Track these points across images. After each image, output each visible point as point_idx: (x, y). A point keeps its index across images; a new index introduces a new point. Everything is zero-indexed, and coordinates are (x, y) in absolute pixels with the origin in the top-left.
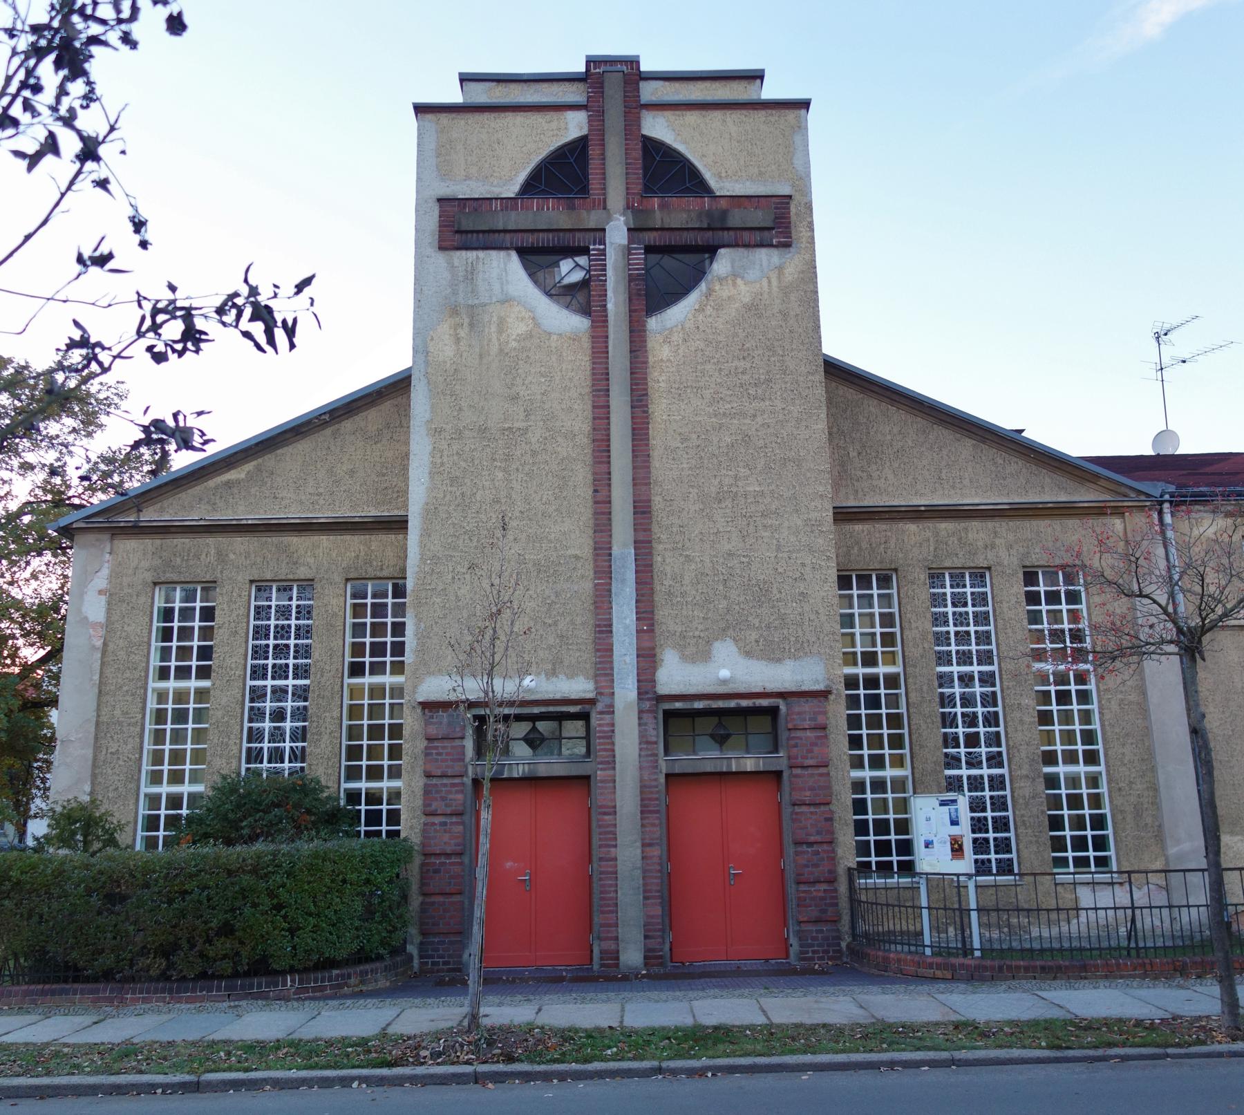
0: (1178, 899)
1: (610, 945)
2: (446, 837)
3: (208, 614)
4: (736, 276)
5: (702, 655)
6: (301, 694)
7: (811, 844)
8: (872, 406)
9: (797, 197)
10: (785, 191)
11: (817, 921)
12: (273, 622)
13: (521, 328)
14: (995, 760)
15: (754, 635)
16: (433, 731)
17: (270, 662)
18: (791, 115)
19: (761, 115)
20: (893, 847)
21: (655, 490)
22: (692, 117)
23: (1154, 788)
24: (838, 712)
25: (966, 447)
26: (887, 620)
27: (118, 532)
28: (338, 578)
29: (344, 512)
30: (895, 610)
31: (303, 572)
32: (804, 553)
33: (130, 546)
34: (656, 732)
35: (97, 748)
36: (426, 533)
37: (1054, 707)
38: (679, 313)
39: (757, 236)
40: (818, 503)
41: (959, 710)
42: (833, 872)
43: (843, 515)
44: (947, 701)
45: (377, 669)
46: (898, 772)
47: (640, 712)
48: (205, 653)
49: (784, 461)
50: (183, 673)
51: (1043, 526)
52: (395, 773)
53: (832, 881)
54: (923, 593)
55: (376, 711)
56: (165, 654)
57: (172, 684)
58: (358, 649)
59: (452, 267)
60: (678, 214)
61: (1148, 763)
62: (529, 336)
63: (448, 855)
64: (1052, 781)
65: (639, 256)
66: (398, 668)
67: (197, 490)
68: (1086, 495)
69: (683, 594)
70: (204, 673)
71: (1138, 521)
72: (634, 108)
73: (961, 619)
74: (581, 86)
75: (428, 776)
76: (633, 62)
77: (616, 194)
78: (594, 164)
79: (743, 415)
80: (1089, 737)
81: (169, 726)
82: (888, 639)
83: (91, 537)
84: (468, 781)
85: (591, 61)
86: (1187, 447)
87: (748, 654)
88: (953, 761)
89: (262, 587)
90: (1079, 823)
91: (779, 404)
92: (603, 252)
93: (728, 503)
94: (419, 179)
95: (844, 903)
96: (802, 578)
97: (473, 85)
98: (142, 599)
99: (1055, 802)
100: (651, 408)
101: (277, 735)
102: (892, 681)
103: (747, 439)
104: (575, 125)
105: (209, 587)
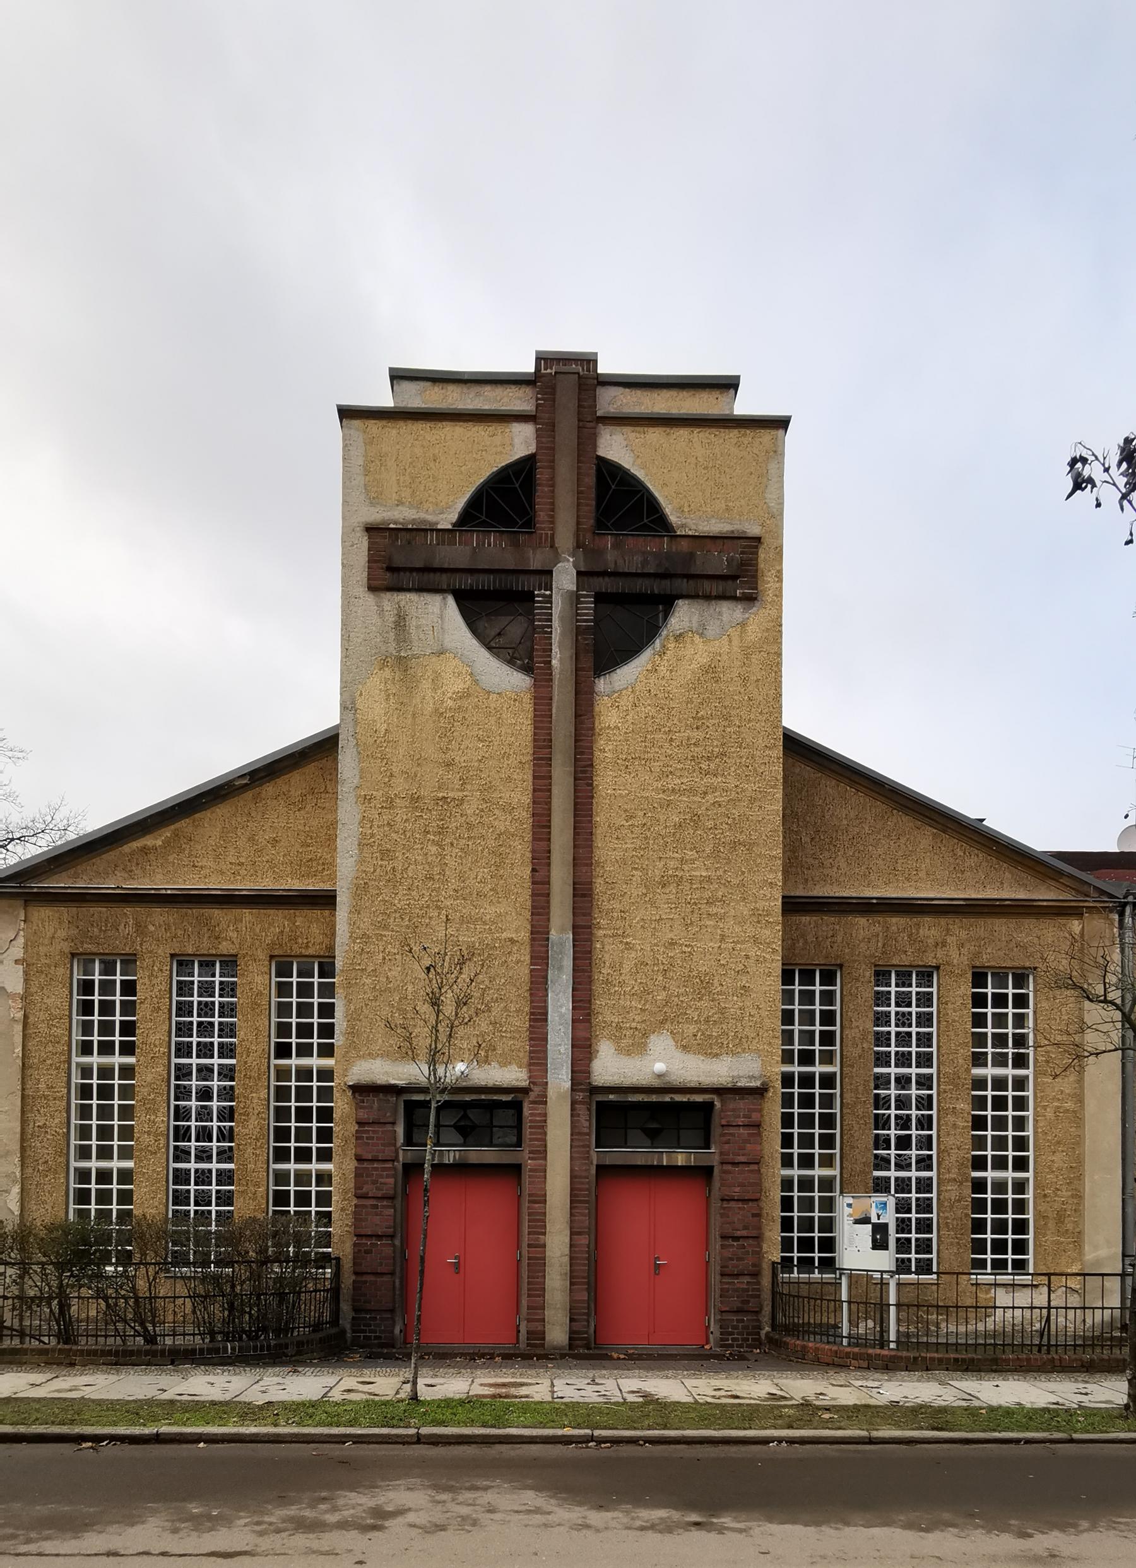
3: (129, 988)
4: (696, 633)
5: (638, 1047)
8: (830, 787)
9: (767, 540)
10: (754, 530)
11: (738, 1311)
13: (459, 686)
14: (924, 1163)
15: (692, 1029)
16: (363, 1115)
17: (195, 1040)
18: (766, 436)
19: (734, 433)
21: (599, 871)
22: (655, 435)
23: (1079, 1196)
24: (773, 1110)
25: (926, 836)
28: (262, 955)
29: (267, 883)
30: (837, 1008)
31: (225, 948)
32: (748, 948)
33: (43, 914)
34: (588, 1122)
35: (24, 1122)
36: (356, 910)
38: (628, 674)
40: (766, 891)
42: (757, 1265)
43: (792, 906)
44: (881, 1102)
45: (305, 1051)
46: (827, 1172)
47: (573, 1103)
49: (735, 845)
50: (106, 1048)
51: (1001, 926)
52: (325, 1155)
53: (756, 1274)
54: (867, 990)
55: (304, 1094)
56: (87, 1028)
57: (95, 1060)
58: (284, 1030)
59: (381, 612)
60: (630, 553)
62: (466, 695)
63: (379, 1237)
64: (979, 1186)
65: (588, 606)
66: (327, 1051)
67: (112, 855)
68: (1045, 894)
69: (621, 984)
70: (128, 1049)
72: (592, 422)
74: (527, 392)
75: (359, 1159)
76: (589, 361)
77: (565, 537)
78: (541, 491)
79: (692, 791)
84: (399, 1166)
85: (543, 359)
89: (184, 963)
91: (732, 782)
93: (672, 888)
94: (345, 502)
95: (767, 1295)
98: (61, 971)
100: (597, 780)
101: (204, 1114)
102: (828, 1081)
104: (520, 441)
105: (129, 962)
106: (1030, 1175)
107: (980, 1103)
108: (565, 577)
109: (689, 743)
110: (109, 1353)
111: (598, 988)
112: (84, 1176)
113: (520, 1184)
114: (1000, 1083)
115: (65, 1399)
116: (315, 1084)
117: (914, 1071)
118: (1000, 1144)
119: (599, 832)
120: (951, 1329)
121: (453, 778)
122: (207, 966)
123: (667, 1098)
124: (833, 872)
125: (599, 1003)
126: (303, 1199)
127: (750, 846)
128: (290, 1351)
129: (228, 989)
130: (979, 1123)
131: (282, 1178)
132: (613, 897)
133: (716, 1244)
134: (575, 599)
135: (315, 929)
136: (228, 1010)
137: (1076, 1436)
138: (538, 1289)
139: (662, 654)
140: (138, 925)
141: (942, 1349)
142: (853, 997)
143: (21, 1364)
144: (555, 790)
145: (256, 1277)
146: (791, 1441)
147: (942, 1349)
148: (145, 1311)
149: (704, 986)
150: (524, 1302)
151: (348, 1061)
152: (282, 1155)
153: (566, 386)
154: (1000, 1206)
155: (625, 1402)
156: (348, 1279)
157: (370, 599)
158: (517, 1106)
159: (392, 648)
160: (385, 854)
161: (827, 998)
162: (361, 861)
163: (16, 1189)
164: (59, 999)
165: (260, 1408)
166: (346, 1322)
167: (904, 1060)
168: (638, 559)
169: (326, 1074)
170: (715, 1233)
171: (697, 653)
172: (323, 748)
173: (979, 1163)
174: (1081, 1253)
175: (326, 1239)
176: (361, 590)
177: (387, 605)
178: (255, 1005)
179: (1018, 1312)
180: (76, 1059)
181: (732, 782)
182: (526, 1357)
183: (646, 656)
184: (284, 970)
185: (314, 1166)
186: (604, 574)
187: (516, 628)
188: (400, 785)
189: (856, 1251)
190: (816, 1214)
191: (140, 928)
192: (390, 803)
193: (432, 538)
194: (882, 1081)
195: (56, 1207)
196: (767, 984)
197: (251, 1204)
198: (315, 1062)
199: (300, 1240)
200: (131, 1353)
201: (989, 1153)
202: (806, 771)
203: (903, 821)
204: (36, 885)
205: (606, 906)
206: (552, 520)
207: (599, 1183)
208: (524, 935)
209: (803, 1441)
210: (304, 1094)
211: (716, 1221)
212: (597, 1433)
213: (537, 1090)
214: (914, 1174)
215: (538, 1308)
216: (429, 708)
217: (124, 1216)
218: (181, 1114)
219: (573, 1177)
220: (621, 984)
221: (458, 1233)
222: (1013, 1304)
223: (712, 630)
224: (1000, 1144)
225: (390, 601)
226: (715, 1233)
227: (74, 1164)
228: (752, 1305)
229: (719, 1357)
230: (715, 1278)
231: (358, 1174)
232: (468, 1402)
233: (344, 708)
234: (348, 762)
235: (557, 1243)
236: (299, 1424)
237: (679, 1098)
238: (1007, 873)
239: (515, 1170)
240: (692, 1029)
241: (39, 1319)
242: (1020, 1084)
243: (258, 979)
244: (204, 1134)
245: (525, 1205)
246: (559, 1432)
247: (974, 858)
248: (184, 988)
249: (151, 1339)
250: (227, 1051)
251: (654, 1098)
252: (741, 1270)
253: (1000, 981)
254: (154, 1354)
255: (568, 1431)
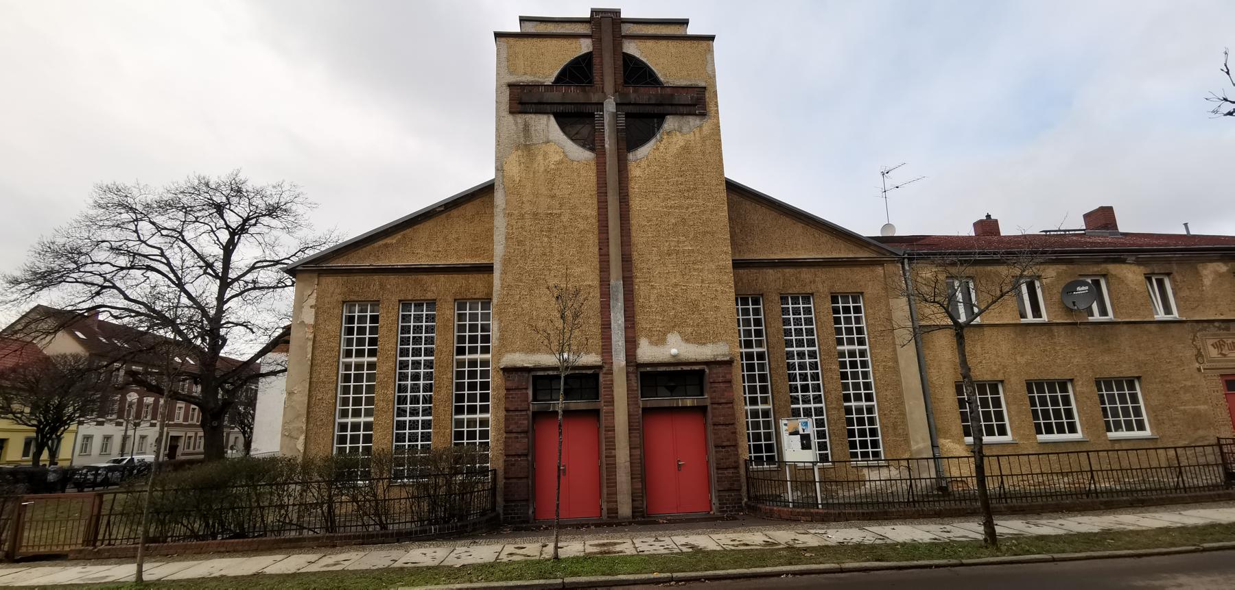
0: (915, 475)
1: (612, 505)
2: (518, 445)
3: (374, 319)
4: (676, 134)
5: (661, 341)
6: (429, 364)
7: (723, 447)
8: (747, 205)
9: (709, 88)
10: (703, 84)
11: (728, 490)
12: (412, 324)
13: (557, 158)
14: (817, 399)
15: (690, 330)
16: (509, 384)
17: (411, 347)
18: (704, 44)
19: (688, 43)
20: (769, 449)
21: (634, 248)
22: (650, 43)
23: (903, 414)
24: (738, 373)
25: (799, 228)
26: (758, 322)
27: (322, 273)
28: (450, 299)
29: (453, 261)
30: (762, 317)
31: (429, 296)
32: (715, 286)
33: (328, 280)
34: (636, 384)
35: (310, 397)
36: (504, 272)
37: (849, 370)
38: (644, 151)
39: (685, 110)
40: (723, 256)
41: (797, 372)
42: (737, 462)
43: (737, 264)
44: (791, 367)
45: (473, 350)
46: (765, 407)
47: (628, 373)
48: (373, 342)
49: (705, 233)
50: (360, 353)
51: (843, 272)
52: (485, 409)
53: (737, 468)
54: (778, 308)
55: (472, 374)
56: (349, 342)
57: (353, 360)
58: (461, 339)
59: (516, 123)
60: (644, 95)
61: (899, 402)
62: (561, 162)
63: (519, 456)
64: (848, 410)
65: (622, 119)
66: (486, 350)
67: (368, 248)
68: (863, 254)
69: (650, 307)
70: (372, 353)
71: (890, 268)
72: (618, 38)
73: (797, 322)
74: (588, 26)
75: (507, 410)
76: (618, 12)
77: (609, 86)
78: (596, 68)
79: (681, 207)
80: (867, 386)
81: (352, 384)
82: (758, 333)
83: (306, 275)
84: (530, 413)
85: (593, 11)
86: (900, 232)
87: (687, 341)
88: (795, 400)
89: (406, 305)
90: (862, 433)
91: (701, 202)
92: (602, 116)
93: (674, 256)
94: (498, 74)
95: (743, 480)
96: (716, 298)
97: (527, 24)
98: (336, 311)
99: (850, 422)
100: (631, 203)
101: (415, 388)
102: (761, 356)
103: (684, 221)
104: (585, 46)
105: (376, 304)
106: (875, 403)
107: (370, 401)
108: (610, 106)
109: (677, 183)
110: (358, 537)
111: (638, 310)
112: (343, 427)
113: (598, 420)
114: (852, 354)
115: (332, 572)
116: (479, 369)
117: (806, 349)
118: (857, 386)
119: (633, 229)
120: (844, 494)
121: (555, 203)
122: (419, 306)
123: (679, 368)
124: (753, 247)
125: (639, 318)
126: (472, 435)
127: (713, 234)
128: (469, 529)
129: (430, 318)
130: (844, 376)
131: (459, 423)
132: (643, 261)
133: (712, 450)
134: (615, 116)
135: (479, 285)
136: (429, 329)
137: (964, 561)
138: (612, 484)
139: (661, 141)
140: (381, 285)
141: (865, 507)
142: (771, 309)
143: (301, 547)
144: (610, 208)
145: (449, 483)
146: (794, 573)
147: (865, 507)
148: (381, 510)
149: (694, 306)
150: (605, 491)
151: (500, 354)
152: (459, 410)
153: (606, 23)
154: (861, 421)
155: (682, 553)
156: (501, 482)
157: (510, 118)
158: (595, 377)
159: (522, 140)
160: (520, 243)
161: (756, 312)
162: (507, 247)
163: (302, 437)
164: (336, 326)
165: (459, 569)
166: (500, 509)
167: (800, 343)
168: (646, 97)
169: (485, 363)
170: (711, 444)
171: (678, 141)
172: (486, 190)
173: (847, 398)
174: (909, 446)
175: (485, 459)
176: (505, 114)
177: (519, 121)
178: (445, 326)
179: (873, 484)
180: (342, 360)
181: (701, 202)
182: (610, 525)
183: (653, 142)
184: (462, 306)
185: (478, 416)
186: (630, 104)
187: (585, 130)
188: (527, 208)
189: (793, 452)
190: (762, 431)
191: (382, 287)
192: (522, 217)
193: (542, 89)
194: (790, 355)
195: (327, 447)
196: (728, 304)
197: (441, 440)
198: (479, 356)
199: (473, 460)
200: (372, 536)
201: (852, 392)
202: (736, 198)
203: (787, 221)
204: (325, 265)
205: (639, 266)
206: (602, 80)
207: (643, 418)
208: (596, 283)
209: (802, 573)
210: (472, 374)
211: (711, 437)
212: (675, 575)
213: (607, 366)
214: (812, 405)
215: (613, 494)
216: (542, 169)
217: (367, 450)
218: (402, 389)
219: (629, 415)
220: (650, 307)
221: (565, 449)
222: (877, 477)
223: (685, 129)
224: (857, 386)
225: (521, 119)
226: (711, 444)
227: (338, 420)
228: (735, 487)
229: (722, 519)
230: (713, 471)
231: (507, 419)
232: (588, 557)
233: (497, 169)
234: (499, 197)
235: (622, 455)
236: (487, 580)
237: (685, 368)
238: (841, 244)
239: (596, 413)
240: (690, 330)
241: (315, 518)
242: (863, 353)
243: (448, 312)
244: (415, 400)
245: (603, 432)
246: (652, 576)
247: (825, 238)
248: (405, 318)
249: (384, 527)
250: (429, 352)
251: (672, 369)
252: (728, 465)
253: (845, 300)
254: (386, 535)
255: (656, 575)
